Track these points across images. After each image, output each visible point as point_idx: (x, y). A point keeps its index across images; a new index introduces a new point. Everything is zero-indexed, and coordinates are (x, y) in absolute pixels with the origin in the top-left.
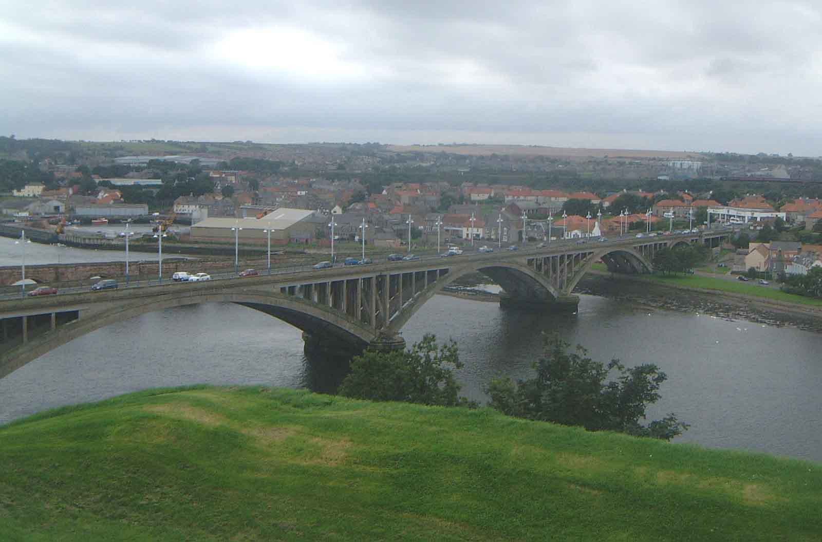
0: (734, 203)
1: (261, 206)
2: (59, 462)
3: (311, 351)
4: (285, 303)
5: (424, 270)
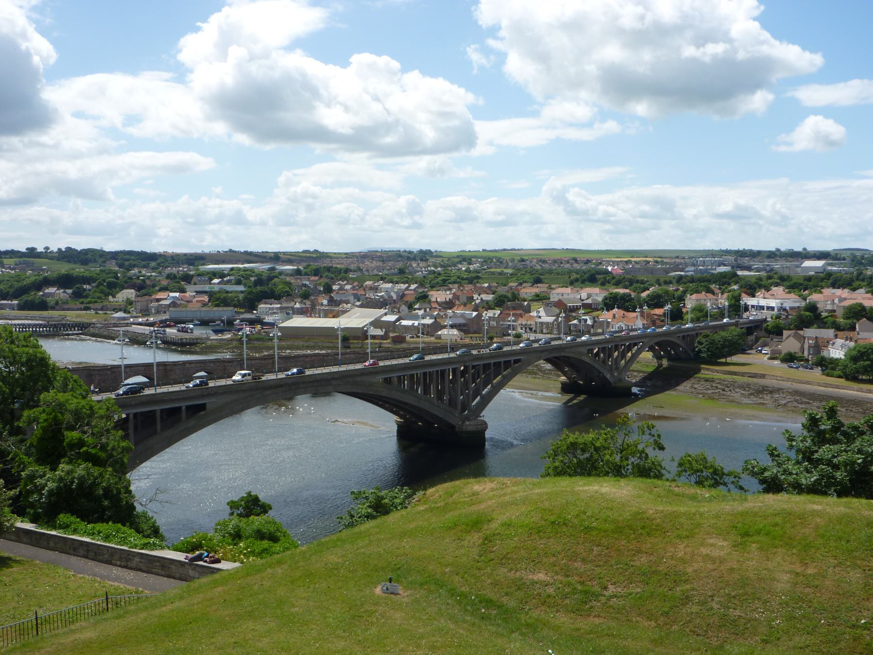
0: (762, 295)
1: (335, 309)
2: (196, 532)
3: (404, 434)
4: (384, 392)
5: (500, 360)
